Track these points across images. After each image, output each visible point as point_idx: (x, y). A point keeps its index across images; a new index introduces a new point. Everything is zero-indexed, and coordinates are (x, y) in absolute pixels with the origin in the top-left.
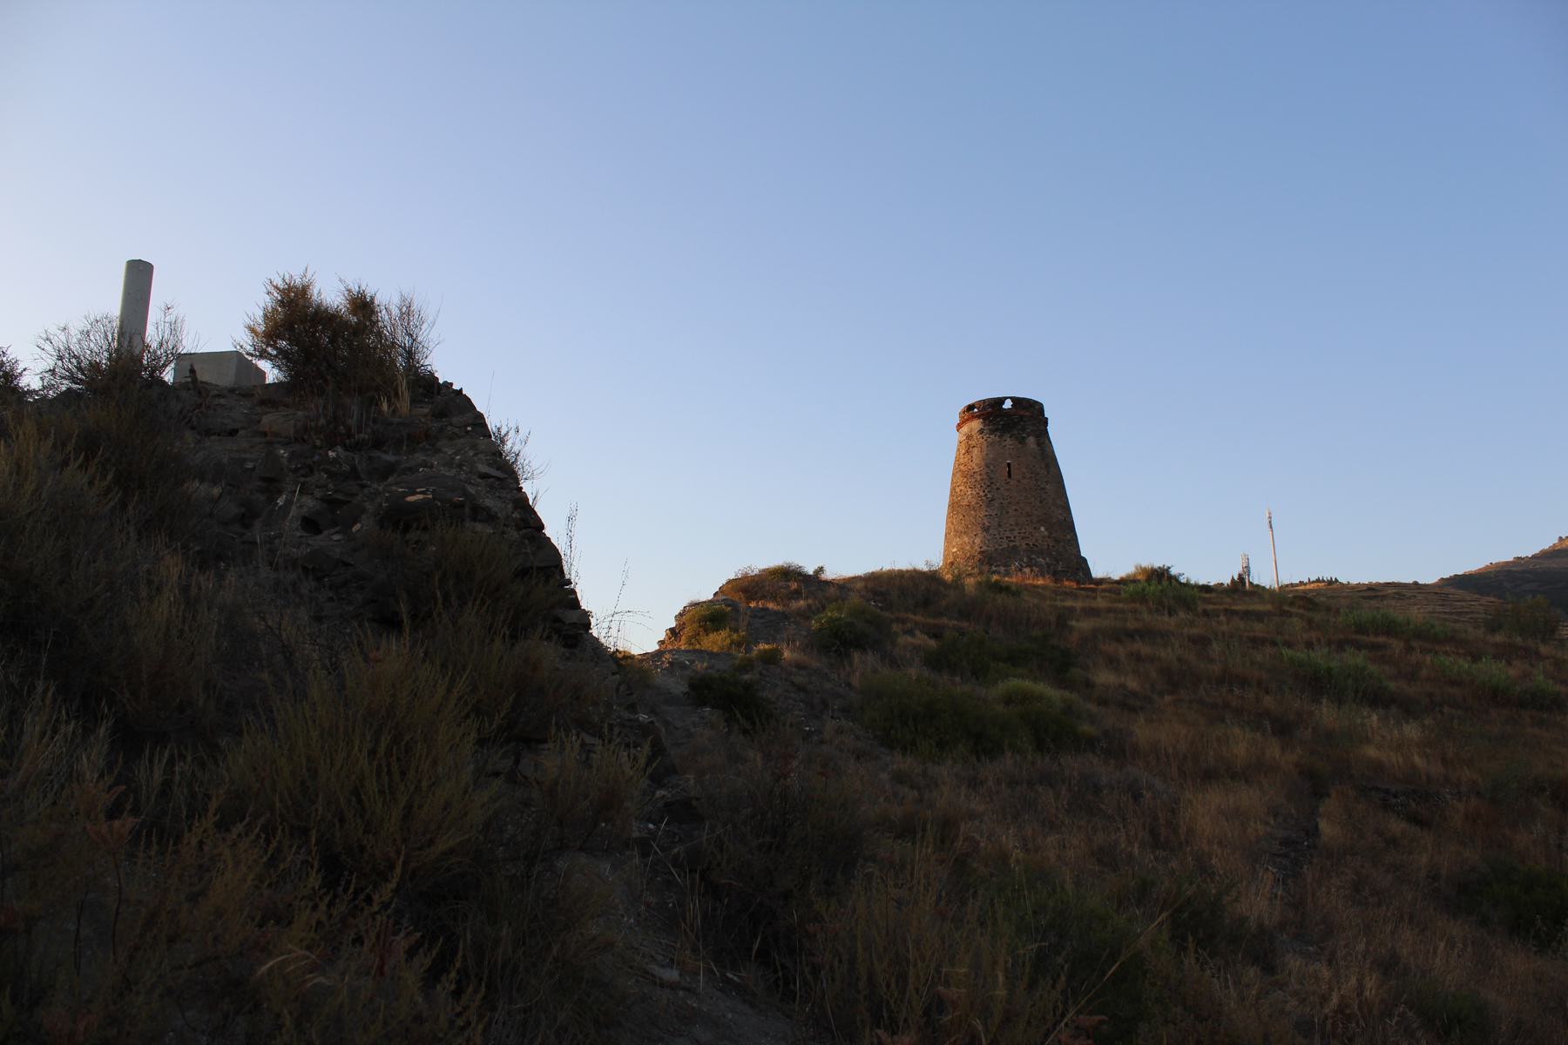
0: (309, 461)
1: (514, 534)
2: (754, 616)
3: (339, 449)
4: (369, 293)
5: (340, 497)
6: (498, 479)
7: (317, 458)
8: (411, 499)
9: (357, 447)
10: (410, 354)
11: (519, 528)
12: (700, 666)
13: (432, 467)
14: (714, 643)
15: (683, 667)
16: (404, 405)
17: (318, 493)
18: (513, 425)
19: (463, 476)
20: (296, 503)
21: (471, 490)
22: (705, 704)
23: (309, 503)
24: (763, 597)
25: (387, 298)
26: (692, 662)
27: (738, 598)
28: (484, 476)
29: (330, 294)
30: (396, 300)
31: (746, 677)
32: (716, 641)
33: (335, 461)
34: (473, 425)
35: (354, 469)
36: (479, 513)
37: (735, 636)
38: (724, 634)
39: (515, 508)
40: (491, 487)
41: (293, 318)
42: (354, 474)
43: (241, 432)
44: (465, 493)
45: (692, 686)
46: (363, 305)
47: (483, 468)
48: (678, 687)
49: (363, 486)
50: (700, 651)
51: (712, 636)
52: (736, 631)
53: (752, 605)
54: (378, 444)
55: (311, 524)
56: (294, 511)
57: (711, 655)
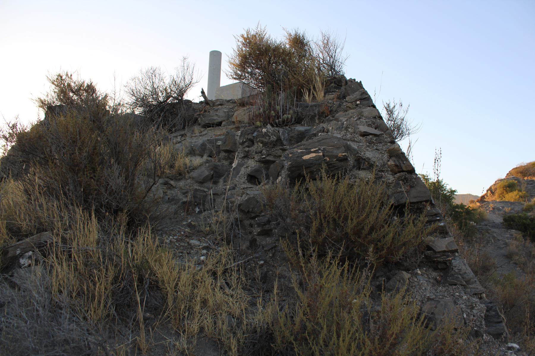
0: (250, 137)
1: (390, 178)
2: (528, 184)
3: (269, 126)
4: (301, 32)
5: (271, 158)
6: (375, 135)
7: (255, 134)
8: (306, 157)
9: (285, 123)
10: (332, 67)
11: (394, 173)
12: (507, 209)
13: (328, 131)
14: (512, 197)
15: (499, 210)
16: (320, 95)
17: (257, 157)
18: (397, 101)
19: (349, 136)
20: (244, 166)
21: (354, 146)
22: (512, 228)
23: (252, 164)
24: (530, 175)
25: (314, 39)
26: (503, 207)
27: (519, 176)
28: (365, 134)
29: (278, 36)
30: (321, 38)
31: (530, 214)
32: (512, 196)
33: (266, 134)
34: (361, 99)
35: (279, 139)
36: (361, 163)
37: (520, 193)
38: (515, 193)
39: (390, 157)
40: (371, 142)
41: (258, 54)
42: (279, 141)
43: (223, 123)
44: (348, 148)
45: (505, 220)
46: (298, 42)
47: (363, 128)
48: (499, 220)
49: (284, 150)
50: (506, 202)
51: (510, 194)
52: (520, 191)
53: (526, 178)
54: (299, 121)
55: (253, 178)
56: (243, 171)
57: (512, 203)
